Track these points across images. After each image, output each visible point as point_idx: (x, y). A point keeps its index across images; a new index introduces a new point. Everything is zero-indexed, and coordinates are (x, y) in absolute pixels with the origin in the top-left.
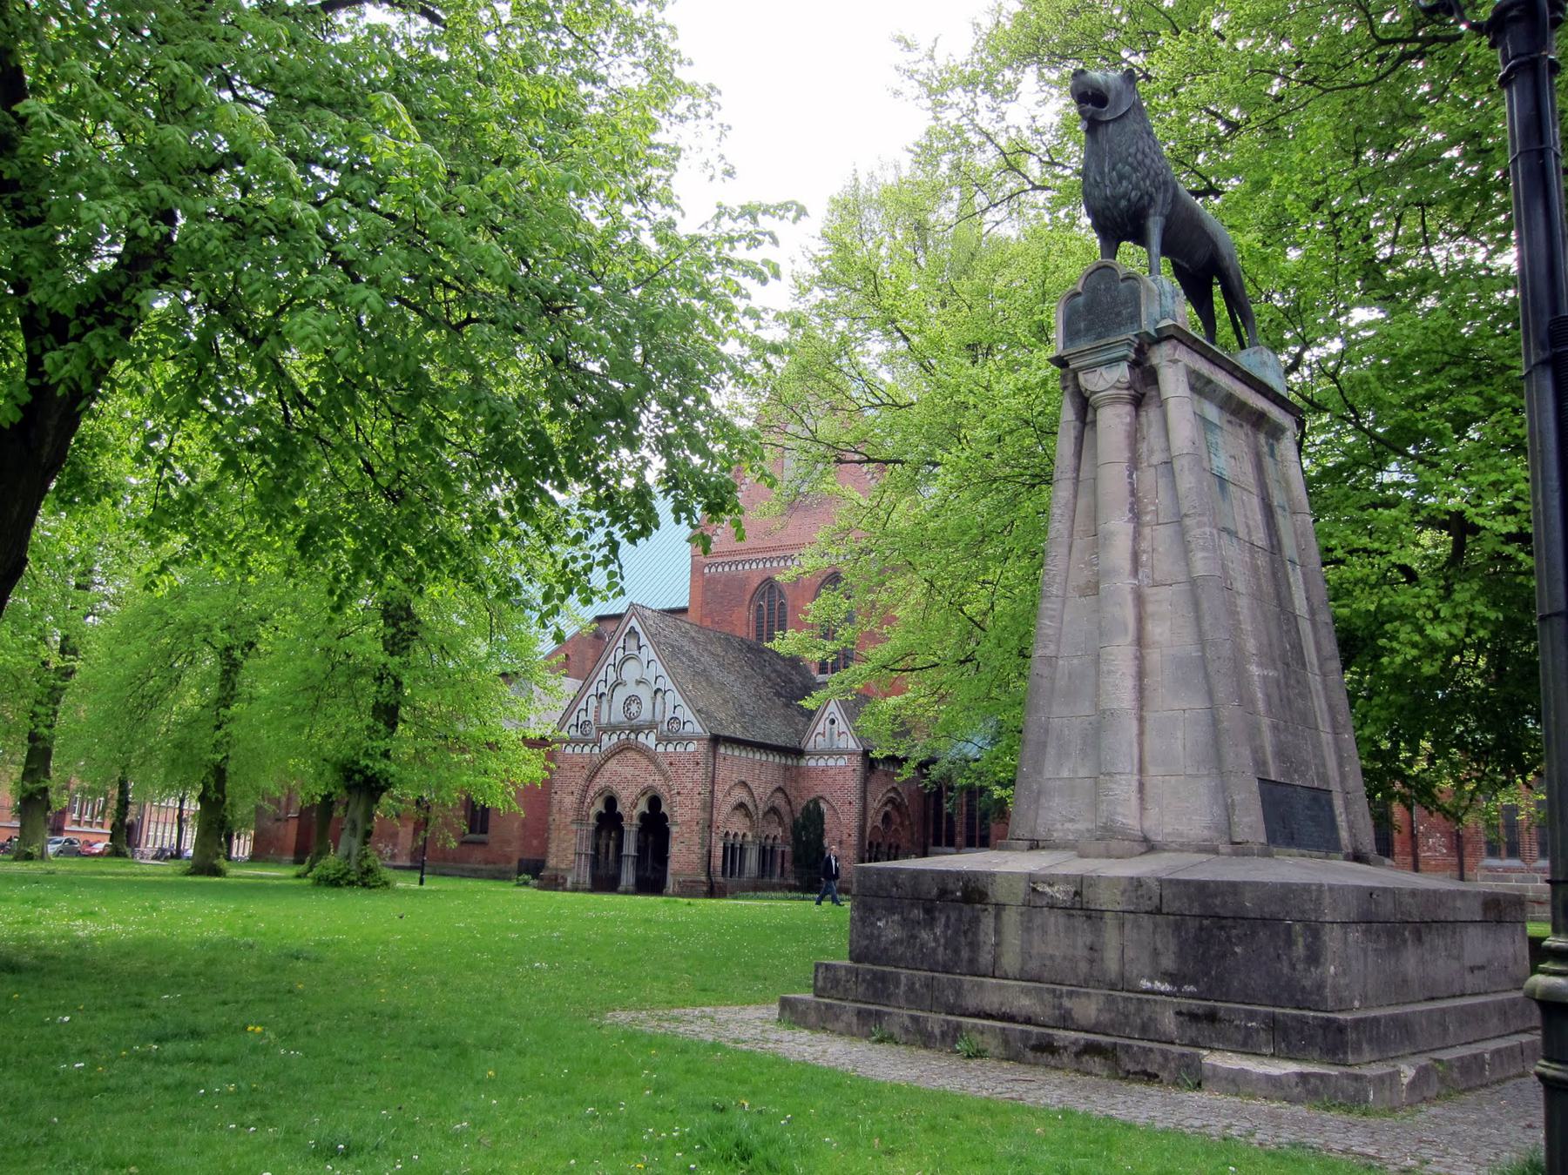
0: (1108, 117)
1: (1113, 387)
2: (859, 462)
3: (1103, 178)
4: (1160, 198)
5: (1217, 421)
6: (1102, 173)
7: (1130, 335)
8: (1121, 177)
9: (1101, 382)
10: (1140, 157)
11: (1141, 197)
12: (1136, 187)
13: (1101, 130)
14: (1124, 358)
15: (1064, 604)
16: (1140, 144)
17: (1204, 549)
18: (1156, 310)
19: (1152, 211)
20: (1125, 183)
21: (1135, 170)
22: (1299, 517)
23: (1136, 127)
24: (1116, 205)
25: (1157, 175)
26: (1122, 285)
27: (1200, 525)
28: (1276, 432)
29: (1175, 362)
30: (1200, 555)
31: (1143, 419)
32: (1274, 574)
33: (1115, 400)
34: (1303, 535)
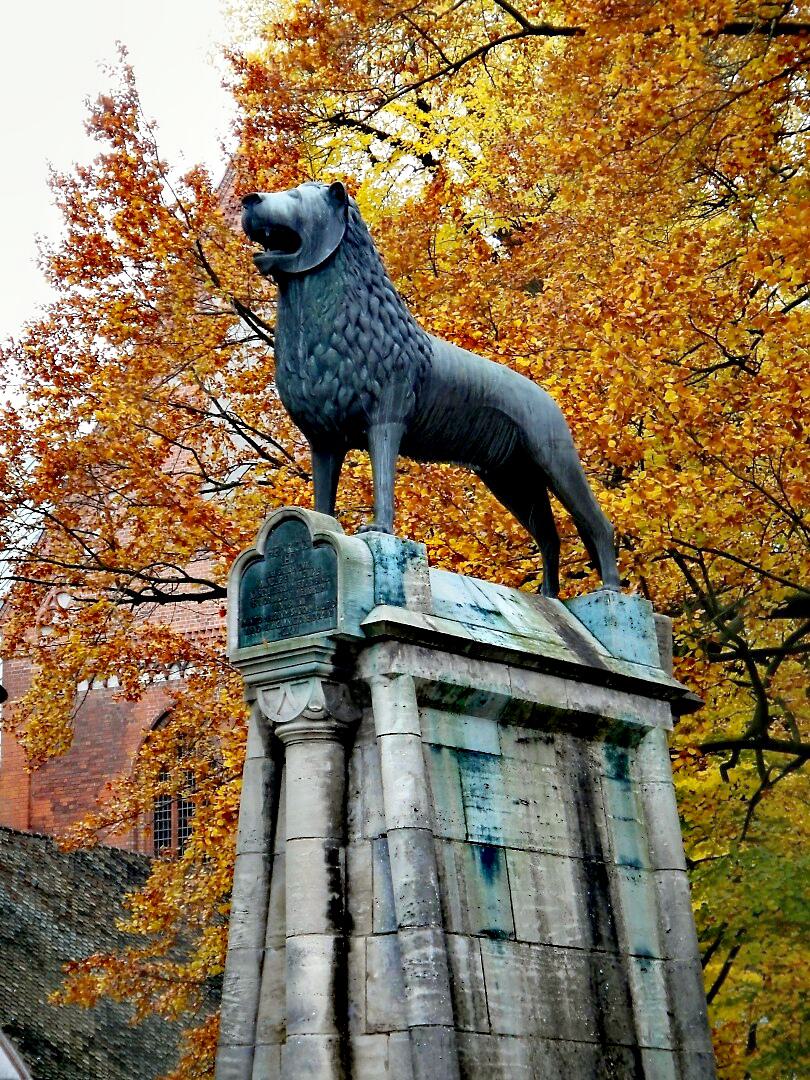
0: (301, 268)
1: (301, 717)
2: (200, 598)
3: (297, 367)
4: (388, 394)
5: (492, 748)
6: (294, 358)
7: (318, 638)
8: (323, 367)
9: (286, 709)
10: (350, 331)
11: (355, 397)
12: (346, 381)
13: (294, 286)
14: (314, 673)
15: (253, 1053)
16: (353, 311)
17: (424, 982)
18: (363, 592)
19: (376, 416)
20: (328, 376)
21: (344, 355)
22: (663, 876)
23: (349, 280)
24: (318, 410)
25: (381, 358)
26: (316, 551)
27: (420, 943)
28: (627, 736)
29: (393, 677)
30: (418, 991)
31: (357, 762)
32: (595, 986)
33: (308, 737)
34: (670, 906)
